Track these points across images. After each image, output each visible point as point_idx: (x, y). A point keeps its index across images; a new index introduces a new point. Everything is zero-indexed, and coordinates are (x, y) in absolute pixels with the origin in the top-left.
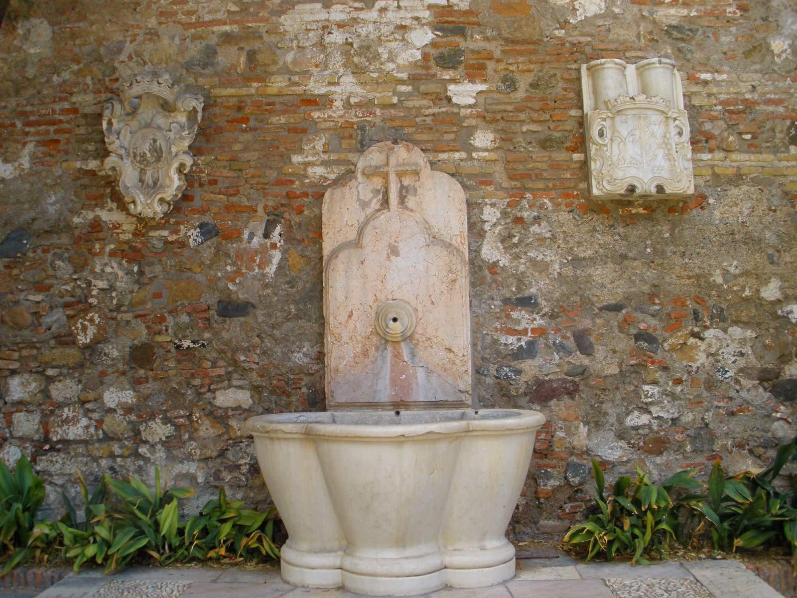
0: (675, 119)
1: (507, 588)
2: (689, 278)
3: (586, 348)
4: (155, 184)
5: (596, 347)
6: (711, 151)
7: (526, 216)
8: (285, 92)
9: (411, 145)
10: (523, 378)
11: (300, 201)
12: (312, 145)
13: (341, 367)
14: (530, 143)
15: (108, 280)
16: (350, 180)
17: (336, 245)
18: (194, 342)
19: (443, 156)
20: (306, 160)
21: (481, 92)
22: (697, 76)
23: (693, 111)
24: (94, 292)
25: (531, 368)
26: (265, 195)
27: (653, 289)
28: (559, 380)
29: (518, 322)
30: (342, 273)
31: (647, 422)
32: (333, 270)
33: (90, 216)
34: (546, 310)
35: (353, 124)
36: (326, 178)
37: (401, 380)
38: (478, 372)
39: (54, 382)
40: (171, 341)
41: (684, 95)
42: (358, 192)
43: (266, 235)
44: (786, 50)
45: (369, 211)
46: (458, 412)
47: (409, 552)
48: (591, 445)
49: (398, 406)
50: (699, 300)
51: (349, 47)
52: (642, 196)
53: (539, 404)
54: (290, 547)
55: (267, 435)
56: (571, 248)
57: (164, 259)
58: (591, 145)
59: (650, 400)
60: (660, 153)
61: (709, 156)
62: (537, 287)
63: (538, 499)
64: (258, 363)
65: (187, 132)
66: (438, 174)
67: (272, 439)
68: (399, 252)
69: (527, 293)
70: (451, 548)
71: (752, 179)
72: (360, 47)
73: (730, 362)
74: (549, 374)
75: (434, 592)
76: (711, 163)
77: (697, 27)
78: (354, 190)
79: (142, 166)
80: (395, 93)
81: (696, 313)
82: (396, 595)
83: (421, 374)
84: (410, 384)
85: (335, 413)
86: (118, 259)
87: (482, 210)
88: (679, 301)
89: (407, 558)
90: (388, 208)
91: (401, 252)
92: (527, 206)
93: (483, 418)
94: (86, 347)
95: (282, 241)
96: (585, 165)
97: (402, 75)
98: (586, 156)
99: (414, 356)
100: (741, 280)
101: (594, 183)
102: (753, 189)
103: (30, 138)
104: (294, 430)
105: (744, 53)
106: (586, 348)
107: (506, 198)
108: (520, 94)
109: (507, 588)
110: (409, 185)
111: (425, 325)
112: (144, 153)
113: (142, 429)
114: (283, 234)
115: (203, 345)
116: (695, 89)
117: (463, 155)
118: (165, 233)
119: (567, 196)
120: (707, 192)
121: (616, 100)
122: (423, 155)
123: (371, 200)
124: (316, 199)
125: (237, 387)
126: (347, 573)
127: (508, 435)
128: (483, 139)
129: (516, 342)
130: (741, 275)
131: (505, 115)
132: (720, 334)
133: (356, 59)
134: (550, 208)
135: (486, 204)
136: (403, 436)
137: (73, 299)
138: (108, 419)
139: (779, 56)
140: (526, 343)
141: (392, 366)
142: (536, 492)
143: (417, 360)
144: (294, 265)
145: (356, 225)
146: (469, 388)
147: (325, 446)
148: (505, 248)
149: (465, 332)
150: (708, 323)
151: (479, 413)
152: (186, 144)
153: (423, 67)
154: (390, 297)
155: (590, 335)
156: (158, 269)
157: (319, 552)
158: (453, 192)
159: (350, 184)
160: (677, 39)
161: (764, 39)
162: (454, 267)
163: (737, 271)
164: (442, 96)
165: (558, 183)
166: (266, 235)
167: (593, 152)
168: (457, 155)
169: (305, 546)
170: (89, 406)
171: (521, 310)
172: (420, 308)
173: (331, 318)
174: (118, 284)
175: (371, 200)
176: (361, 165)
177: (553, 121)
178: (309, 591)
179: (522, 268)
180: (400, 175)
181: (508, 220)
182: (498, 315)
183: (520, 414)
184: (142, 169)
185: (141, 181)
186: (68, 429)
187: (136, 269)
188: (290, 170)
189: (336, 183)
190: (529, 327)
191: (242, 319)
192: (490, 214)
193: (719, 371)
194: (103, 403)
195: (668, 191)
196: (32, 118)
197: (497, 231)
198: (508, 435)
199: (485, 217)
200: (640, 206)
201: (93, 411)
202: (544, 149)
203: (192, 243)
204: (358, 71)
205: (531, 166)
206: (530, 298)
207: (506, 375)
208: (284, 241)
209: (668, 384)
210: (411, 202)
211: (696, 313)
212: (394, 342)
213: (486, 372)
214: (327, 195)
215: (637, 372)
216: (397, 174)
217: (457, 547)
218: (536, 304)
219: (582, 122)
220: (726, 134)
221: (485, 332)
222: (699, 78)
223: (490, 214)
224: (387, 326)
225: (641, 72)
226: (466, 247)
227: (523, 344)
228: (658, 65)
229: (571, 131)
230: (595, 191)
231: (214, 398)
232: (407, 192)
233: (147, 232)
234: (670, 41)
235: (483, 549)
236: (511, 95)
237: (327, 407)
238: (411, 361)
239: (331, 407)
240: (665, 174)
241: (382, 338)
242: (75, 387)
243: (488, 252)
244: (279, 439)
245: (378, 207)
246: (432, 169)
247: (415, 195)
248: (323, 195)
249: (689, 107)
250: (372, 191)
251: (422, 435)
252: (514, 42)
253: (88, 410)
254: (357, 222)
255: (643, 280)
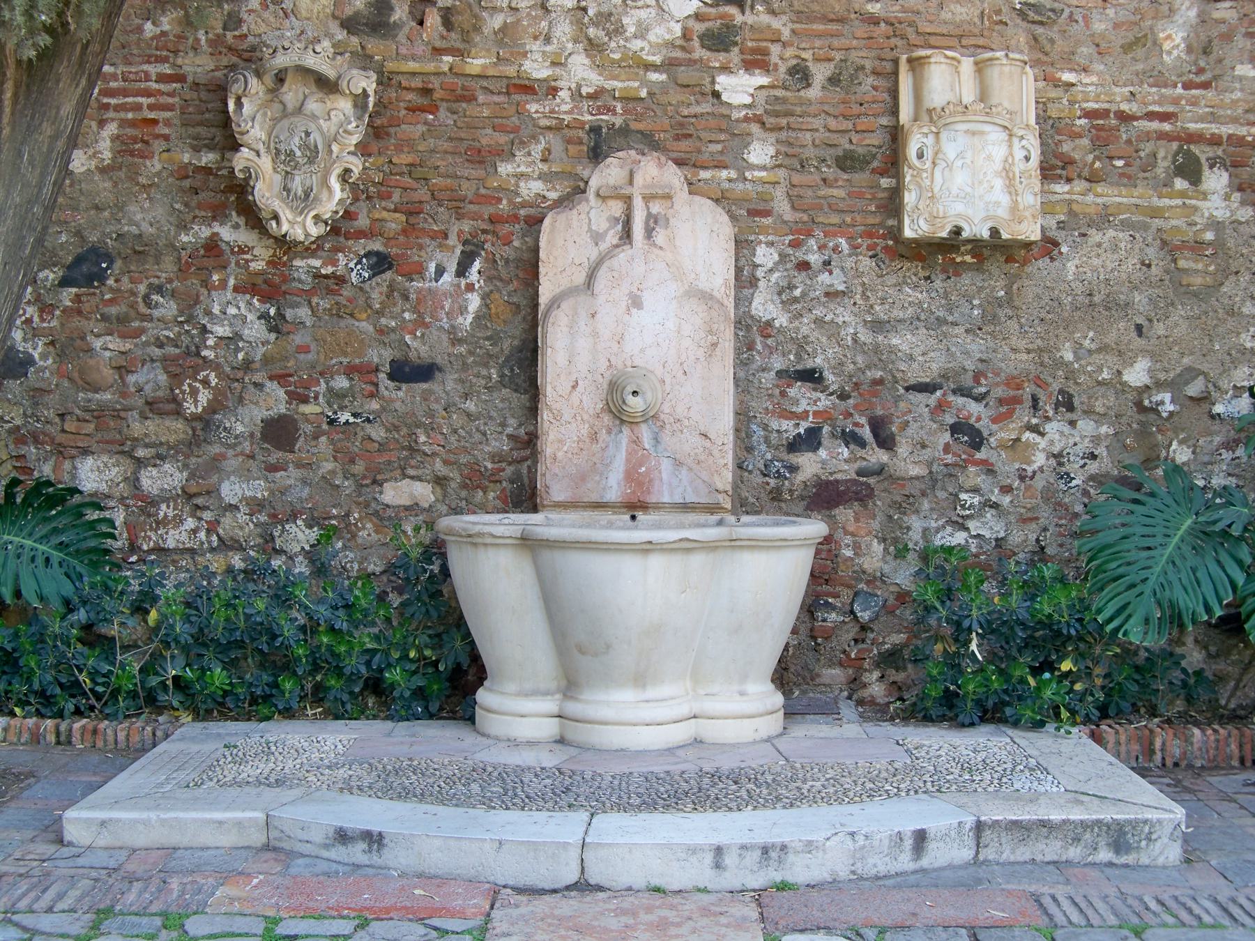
0: (1022, 138)
2: (1029, 352)
3: (886, 441)
4: (307, 195)
5: (898, 438)
6: (1069, 180)
8: (491, 72)
10: (800, 477)
13: (560, 455)
14: (824, 161)
15: (231, 325)
16: (579, 203)
17: (558, 291)
18: (355, 415)
19: (704, 174)
20: (518, 170)
21: (762, 87)
22: (1058, 76)
23: (1050, 127)
24: (210, 342)
25: (810, 465)
26: (460, 217)
27: (980, 365)
28: (847, 481)
29: (797, 402)
30: (565, 329)
31: (963, 542)
33: (205, 232)
34: (833, 387)
35: (584, 123)
38: (740, 467)
39: (146, 467)
40: (322, 413)
41: (1037, 102)
43: (462, 271)
44: (1178, 46)
45: (604, 246)
48: (887, 569)
49: (634, 507)
50: (1039, 382)
51: (580, 13)
52: (969, 241)
54: (490, 690)
56: (872, 307)
57: (315, 300)
58: (906, 169)
59: (968, 512)
60: (999, 183)
61: (1067, 188)
65: (354, 124)
66: (697, 198)
67: (475, 545)
69: (809, 364)
70: (702, 692)
71: (1122, 222)
72: (599, 14)
73: (1077, 466)
76: (1067, 197)
77: (1062, 6)
78: (583, 216)
79: (288, 169)
80: (644, 83)
81: (1035, 399)
83: (666, 465)
84: (651, 481)
85: (550, 516)
86: (248, 297)
88: (1014, 382)
90: (631, 243)
93: (746, 525)
94: (196, 417)
96: (896, 194)
97: (654, 58)
98: (898, 183)
100: (1098, 358)
101: (907, 221)
102: (1121, 235)
103: (111, 114)
105: (1122, 47)
106: (886, 441)
108: (814, 92)
112: (292, 151)
113: (276, 534)
115: (368, 420)
116: (1053, 94)
118: (316, 263)
119: (870, 235)
120: (1059, 236)
121: (943, 109)
123: (606, 232)
125: (412, 478)
127: (780, 547)
128: (760, 153)
130: (1099, 350)
131: (792, 119)
132: (1067, 429)
133: (592, 32)
134: (846, 252)
135: (760, 242)
136: (650, 542)
137: (177, 351)
138: (227, 521)
139: (1169, 53)
141: (629, 454)
142: (812, 630)
143: (660, 448)
146: (729, 488)
147: (546, 555)
148: (782, 302)
150: (1051, 413)
152: (355, 139)
153: (683, 48)
154: (629, 363)
155: (891, 423)
156: (303, 313)
160: (1033, 22)
161: (1151, 29)
163: (1093, 346)
164: (708, 89)
165: (858, 218)
166: (462, 271)
167: (908, 179)
168: (724, 174)
169: (511, 687)
170: (199, 501)
172: (668, 381)
173: (549, 389)
174: (246, 332)
175: (606, 232)
176: (594, 183)
179: (805, 330)
180: (648, 198)
181: (789, 266)
183: (795, 522)
184: (287, 173)
185: (286, 189)
186: (167, 533)
187: (272, 312)
189: (559, 204)
190: (811, 409)
191: (425, 386)
192: (765, 256)
193: (1062, 478)
194: (220, 498)
195: (1005, 236)
196: (113, 84)
198: (780, 547)
199: (758, 260)
200: (968, 253)
201: (206, 508)
202: (843, 170)
203: (354, 278)
204: (593, 48)
206: (813, 371)
207: (778, 472)
209: (992, 492)
210: (660, 237)
211: (1035, 399)
213: (750, 467)
215: (951, 475)
218: (820, 380)
219: (896, 135)
220: (1090, 157)
222: (1060, 80)
223: (765, 256)
224: (624, 402)
225: (980, 67)
226: (732, 299)
227: (802, 430)
228: (1004, 61)
229: (880, 147)
230: (908, 233)
231: (381, 493)
232: (656, 222)
233: (291, 260)
234: (1024, 24)
235: (742, 694)
236: (802, 93)
239: (544, 506)
240: (1003, 212)
242: (177, 474)
243: (761, 308)
244: (485, 545)
245: (615, 241)
248: (541, 221)
249: (1042, 119)
251: (674, 542)
252: (811, 18)
253: (197, 507)
255: (967, 353)
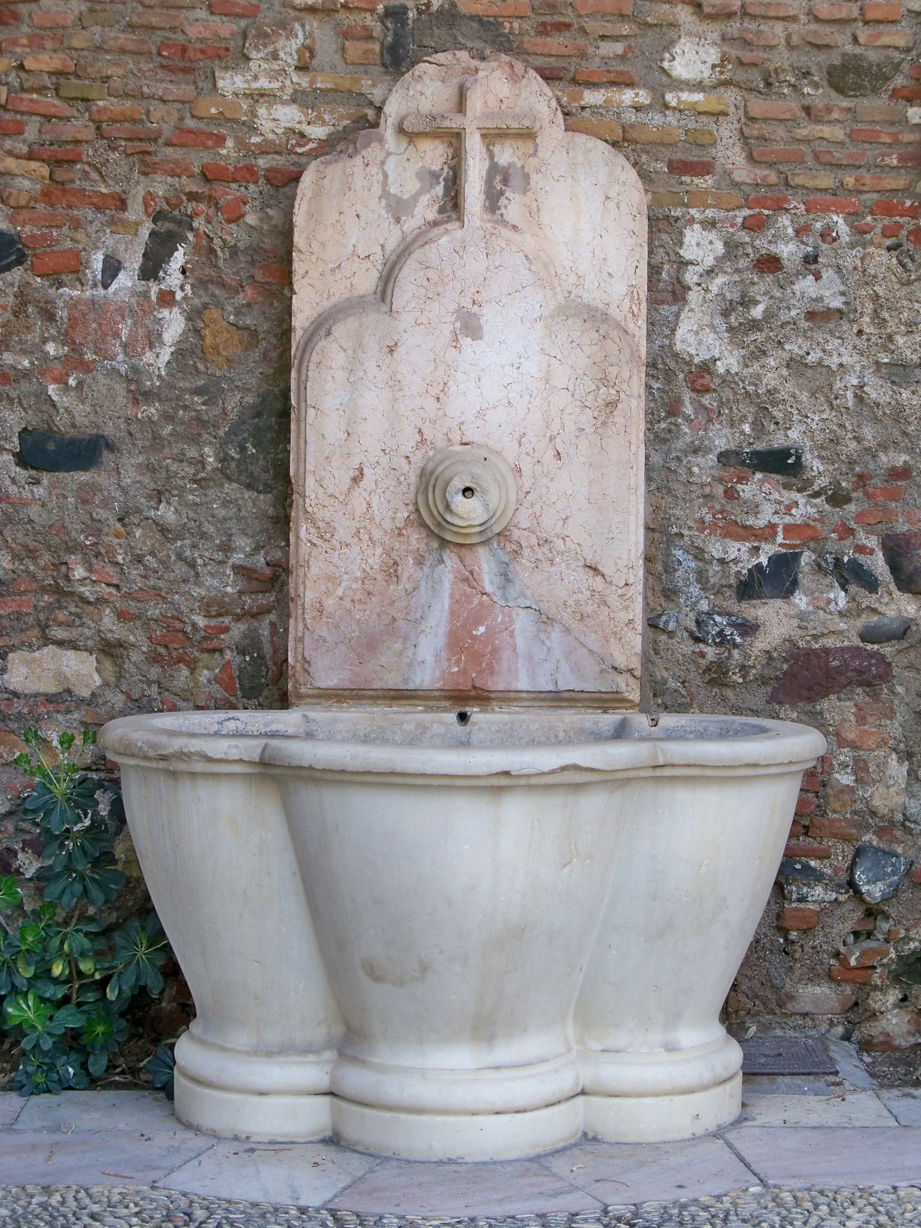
1: (730, 1145)
7: (785, 255)
9: (519, 66)
10: (761, 644)
11: (233, 191)
12: (270, 49)
16: (366, 146)
17: (327, 304)
19: (592, 97)
29: (755, 509)
30: (341, 375)
32: (319, 364)
36: (302, 135)
37: (474, 638)
42: (386, 176)
45: (412, 224)
46: (610, 720)
47: (503, 1052)
53: (793, 705)
55: (162, 765)
56: (890, 338)
62: (803, 428)
63: (783, 931)
64: (117, 587)
68: (480, 328)
69: (778, 441)
74: (823, 635)
75: (557, 1152)
78: (374, 169)
82: (469, 1159)
83: (523, 623)
84: (495, 651)
85: (312, 715)
87: (681, 234)
89: (497, 1068)
90: (460, 219)
91: (486, 329)
92: (790, 231)
93: (671, 736)
95: (188, 288)
99: (508, 580)
104: (234, 754)
107: (739, 207)
109: (730, 1145)
110: (510, 165)
111: (537, 508)
114: (192, 271)
117: (644, 97)
122: (547, 89)
123: (415, 198)
124: (277, 188)
125: (60, 643)
126: (344, 1105)
129: (745, 556)
134: (845, 239)
136: (507, 774)
140: (770, 559)
143: (512, 592)
144: (216, 348)
145: (379, 256)
146: (636, 663)
148: (731, 329)
149: (633, 529)
151: (661, 722)
154: (456, 437)
157: (279, 1053)
158: (617, 188)
159: (364, 153)
162: (614, 370)
168: (628, 96)
169: (241, 1039)
171: (762, 482)
172: (526, 467)
173: (310, 483)
175: (415, 198)
176: (393, 109)
177: (866, 23)
178: (253, 1150)
179: (770, 380)
180: (491, 137)
181: (742, 263)
182: (707, 490)
183: (763, 730)
188: (213, 111)
191: (83, 477)
197: (714, 287)
199: (687, 253)
205: (805, 132)
206: (785, 453)
207: (721, 633)
208: (193, 286)
212: (462, 545)
214: (307, 179)
216: (484, 136)
217: (609, 1043)
221: (675, 530)
224: (448, 507)
232: (505, 181)
237: (292, 699)
238: (499, 593)
239: (300, 697)
241: (431, 533)
243: (691, 339)
244: (193, 775)
245: (432, 215)
246: (566, 130)
247: (525, 191)
248: (295, 178)
250: (419, 175)
254: (378, 249)
